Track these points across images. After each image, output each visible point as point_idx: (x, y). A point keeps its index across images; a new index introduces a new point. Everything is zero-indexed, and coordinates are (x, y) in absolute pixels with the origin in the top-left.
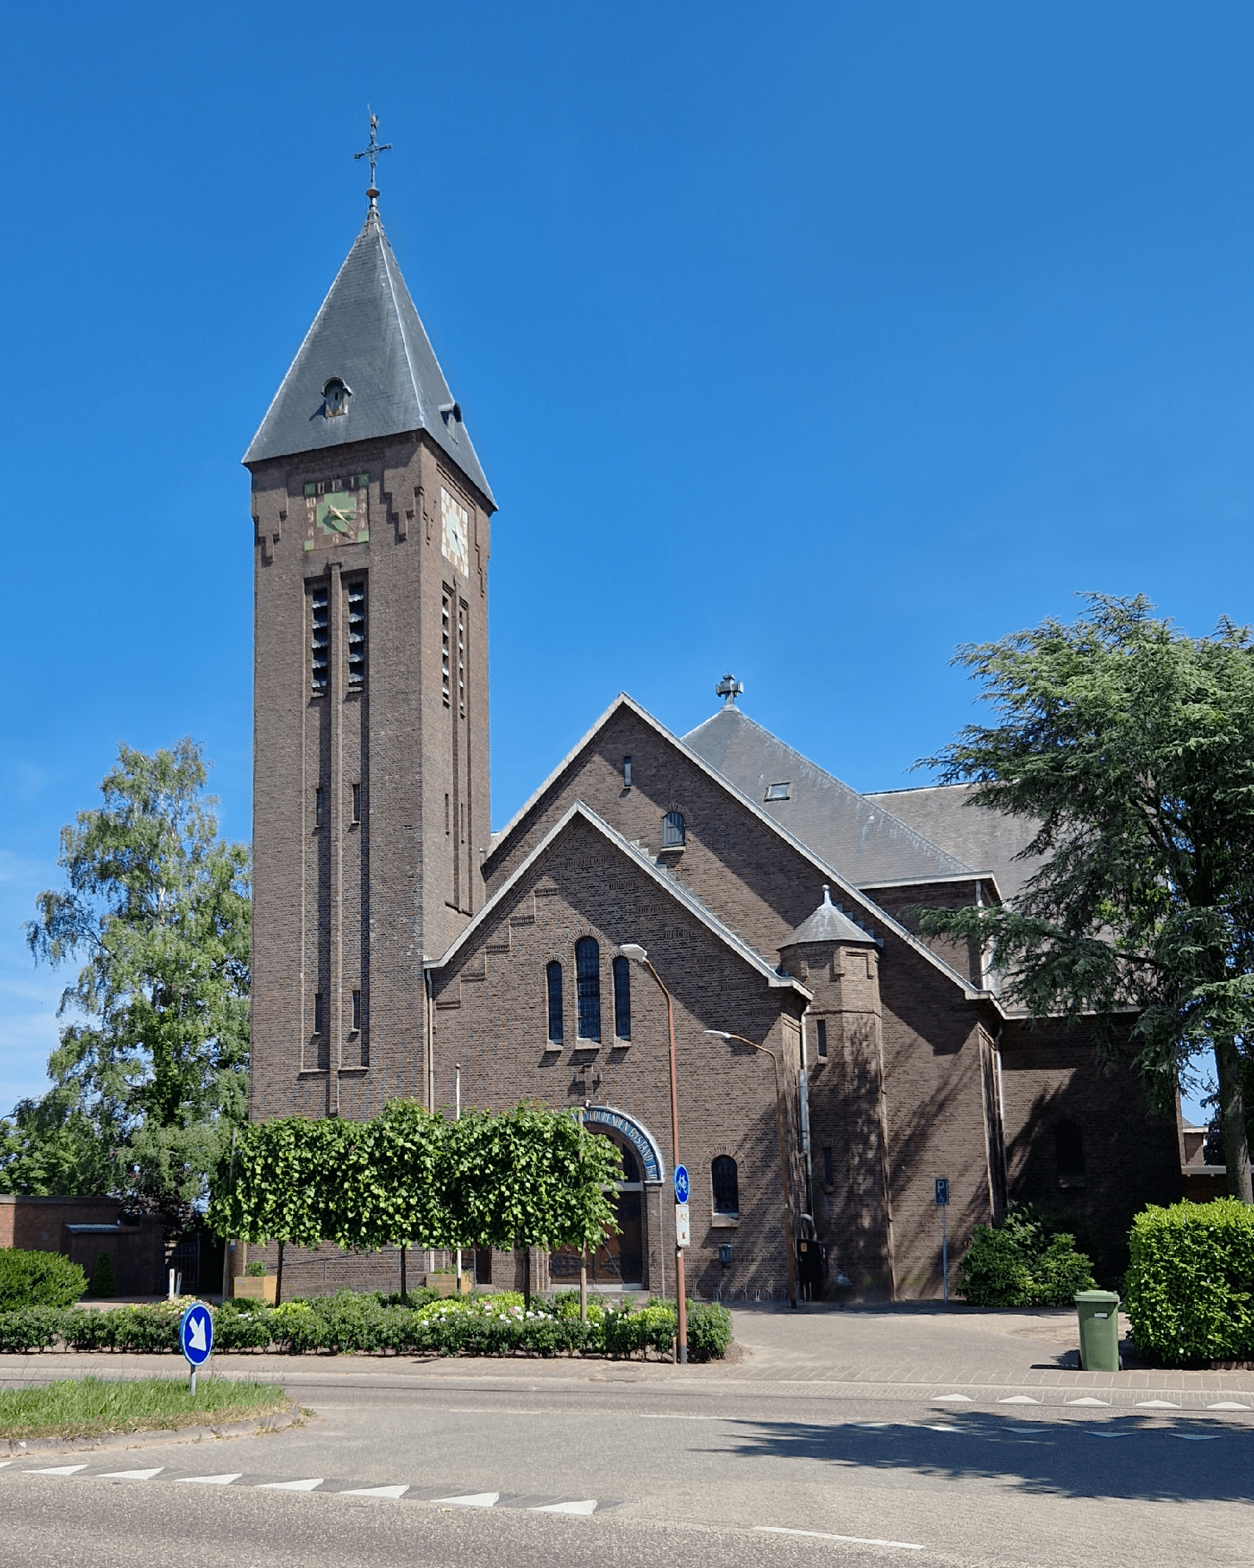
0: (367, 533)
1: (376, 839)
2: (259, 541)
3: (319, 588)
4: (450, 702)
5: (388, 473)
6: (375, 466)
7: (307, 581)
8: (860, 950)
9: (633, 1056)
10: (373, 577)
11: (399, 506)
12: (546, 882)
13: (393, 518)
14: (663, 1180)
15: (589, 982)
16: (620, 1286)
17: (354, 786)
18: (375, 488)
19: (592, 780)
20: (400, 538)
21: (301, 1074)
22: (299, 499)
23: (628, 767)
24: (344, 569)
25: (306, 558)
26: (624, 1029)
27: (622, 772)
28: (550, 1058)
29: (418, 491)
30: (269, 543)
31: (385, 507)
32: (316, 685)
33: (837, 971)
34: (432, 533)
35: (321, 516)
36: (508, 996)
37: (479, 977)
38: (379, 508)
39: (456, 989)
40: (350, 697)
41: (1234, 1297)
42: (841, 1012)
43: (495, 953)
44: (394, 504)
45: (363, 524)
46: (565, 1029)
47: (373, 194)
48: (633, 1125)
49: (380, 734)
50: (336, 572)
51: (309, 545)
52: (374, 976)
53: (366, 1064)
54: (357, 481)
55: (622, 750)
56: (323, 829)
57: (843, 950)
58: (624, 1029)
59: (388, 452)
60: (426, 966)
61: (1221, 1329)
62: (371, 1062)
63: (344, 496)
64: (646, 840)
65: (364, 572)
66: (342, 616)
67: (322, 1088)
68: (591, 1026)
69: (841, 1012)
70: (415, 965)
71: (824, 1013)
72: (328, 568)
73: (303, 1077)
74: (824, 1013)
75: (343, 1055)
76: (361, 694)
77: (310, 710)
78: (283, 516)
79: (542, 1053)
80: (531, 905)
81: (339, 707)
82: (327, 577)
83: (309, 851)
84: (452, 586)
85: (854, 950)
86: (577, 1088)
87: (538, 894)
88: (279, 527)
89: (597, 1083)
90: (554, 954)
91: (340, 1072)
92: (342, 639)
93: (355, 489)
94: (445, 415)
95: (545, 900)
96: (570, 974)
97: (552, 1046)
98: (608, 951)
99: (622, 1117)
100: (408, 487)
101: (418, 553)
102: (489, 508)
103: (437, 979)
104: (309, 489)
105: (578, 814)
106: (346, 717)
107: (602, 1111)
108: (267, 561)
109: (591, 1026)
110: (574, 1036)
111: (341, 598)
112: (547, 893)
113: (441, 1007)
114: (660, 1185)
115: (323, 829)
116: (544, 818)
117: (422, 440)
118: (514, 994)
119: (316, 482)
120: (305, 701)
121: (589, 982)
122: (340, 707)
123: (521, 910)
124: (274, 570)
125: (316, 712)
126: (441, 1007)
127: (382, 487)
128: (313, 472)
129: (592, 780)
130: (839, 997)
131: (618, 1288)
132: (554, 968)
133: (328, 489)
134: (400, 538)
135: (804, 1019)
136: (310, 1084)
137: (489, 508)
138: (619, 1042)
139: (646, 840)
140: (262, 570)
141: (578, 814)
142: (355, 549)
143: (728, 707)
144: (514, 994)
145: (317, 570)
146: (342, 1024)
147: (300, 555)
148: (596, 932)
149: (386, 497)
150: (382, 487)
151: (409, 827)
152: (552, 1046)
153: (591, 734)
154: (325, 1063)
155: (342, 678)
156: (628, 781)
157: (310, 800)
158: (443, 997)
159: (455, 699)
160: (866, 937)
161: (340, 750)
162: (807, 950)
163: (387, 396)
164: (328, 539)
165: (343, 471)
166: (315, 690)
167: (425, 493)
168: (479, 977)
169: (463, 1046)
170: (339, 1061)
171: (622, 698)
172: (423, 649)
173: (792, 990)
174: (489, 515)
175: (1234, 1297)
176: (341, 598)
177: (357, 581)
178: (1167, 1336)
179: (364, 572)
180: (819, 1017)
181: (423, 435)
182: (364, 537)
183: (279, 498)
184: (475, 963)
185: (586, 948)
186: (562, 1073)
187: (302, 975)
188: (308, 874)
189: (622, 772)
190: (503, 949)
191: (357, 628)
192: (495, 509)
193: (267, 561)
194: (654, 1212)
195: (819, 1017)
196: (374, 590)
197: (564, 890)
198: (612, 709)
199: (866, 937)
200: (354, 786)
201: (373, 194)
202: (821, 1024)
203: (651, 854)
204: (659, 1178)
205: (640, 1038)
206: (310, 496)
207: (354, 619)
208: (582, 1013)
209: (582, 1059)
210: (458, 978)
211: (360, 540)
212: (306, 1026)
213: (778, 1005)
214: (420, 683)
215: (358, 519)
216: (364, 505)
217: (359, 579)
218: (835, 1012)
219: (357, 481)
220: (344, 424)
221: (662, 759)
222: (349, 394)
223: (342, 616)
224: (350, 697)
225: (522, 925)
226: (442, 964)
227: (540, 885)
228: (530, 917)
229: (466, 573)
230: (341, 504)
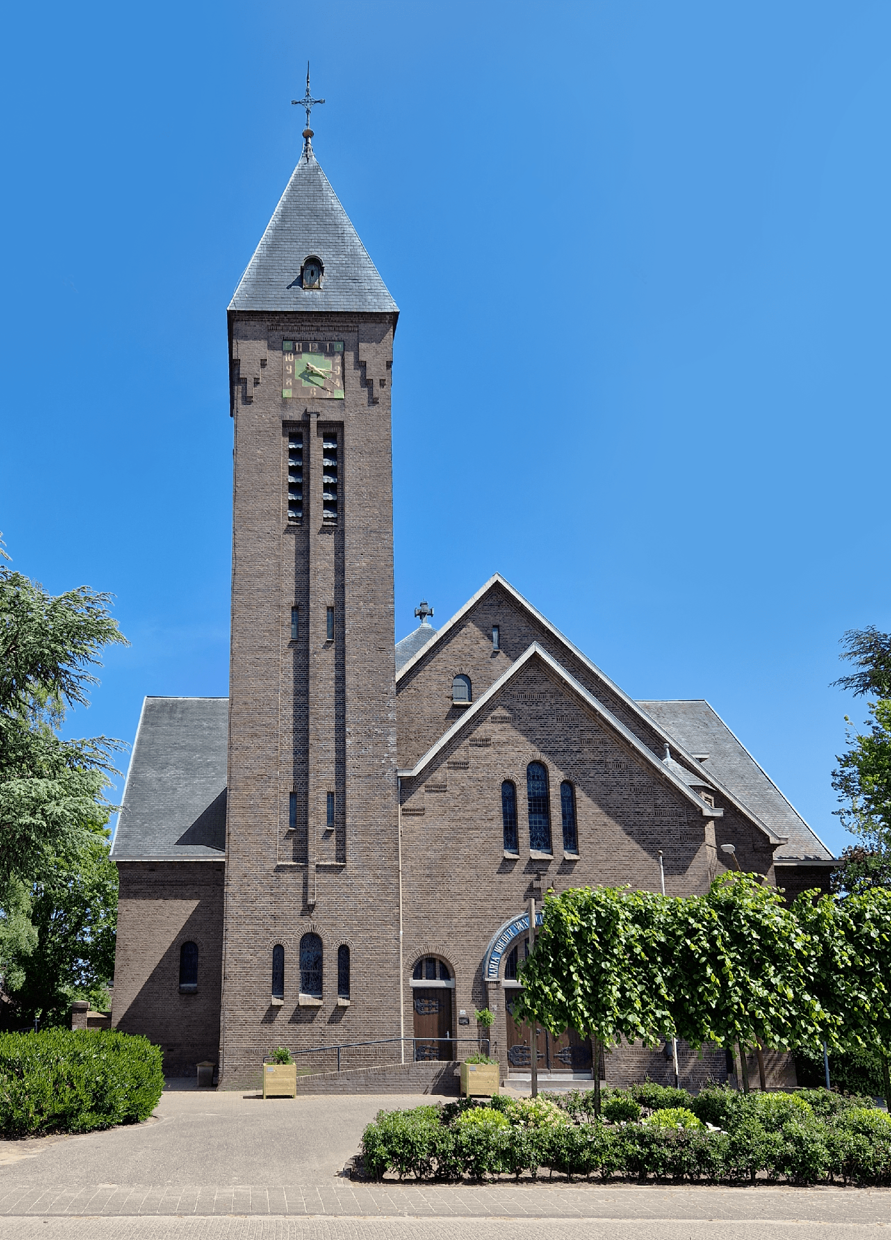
1: (351, 656)
3: (296, 431)
5: (362, 345)
6: (351, 337)
7: (286, 424)
10: (347, 431)
11: (373, 372)
12: (500, 712)
13: (367, 383)
15: (540, 804)
16: (572, 1075)
17: (328, 608)
18: (350, 357)
19: (467, 642)
20: (373, 401)
21: (278, 866)
22: (278, 353)
23: (495, 634)
24: (321, 418)
25: (285, 401)
27: (490, 637)
28: (507, 865)
29: (389, 365)
31: (359, 373)
32: (291, 514)
35: (299, 370)
36: (468, 808)
37: (441, 788)
38: (353, 375)
39: (418, 798)
43: (455, 768)
44: (368, 372)
45: (338, 383)
49: (356, 564)
50: (313, 420)
51: (287, 393)
52: (351, 782)
54: (331, 346)
55: (492, 620)
59: (363, 327)
62: (348, 858)
63: (322, 358)
65: (341, 425)
66: (318, 461)
67: (300, 881)
68: (542, 839)
72: (307, 415)
73: (279, 869)
75: (321, 851)
76: (336, 528)
78: (263, 363)
79: (501, 860)
82: (305, 423)
87: (494, 720)
88: (260, 373)
90: (509, 774)
91: (317, 866)
93: (331, 354)
95: (500, 726)
97: (509, 855)
98: (556, 776)
100: (381, 360)
104: (288, 345)
105: (535, 654)
111: (318, 446)
112: (503, 720)
113: (406, 813)
116: (427, 668)
118: (474, 805)
119: (294, 340)
121: (540, 804)
125: (291, 542)
127: (357, 356)
128: (292, 331)
129: (467, 642)
131: (569, 1077)
132: (509, 786)
133: (306, 350)
134: (373, 401)
136: (287, 878)
141: (535, 654)
142: (331, 403)
144: (474, 805)
146: (318, 823)
147: (279, 400)
148: (545, 759)
149: (361, 365)
150: (357, 356)
151: (381, 649)
153: (471, 603)
154: (302, 856)
155: (319, 515)
156: (496, 645)
164: (306, 390)
165: (320, 336)
166: (290, 519)
168: (441, 788)
169: (427, 850)
171: (496, 578)
176: (318, 446)
177: (333, 431)
179: (341, 425)
182: (339, 394)
184: (438, 776)
185: (537, 772)
186: (518, 880)
188: (287, 681)
189: (490, 637)
190: (464, 766)
197: (515, 719)
198: (489, 585)
200: (328, 608)
205: (587, 852)
206: (288, 352)
207: (328, 463)
209: (536, 868)
210: (422, 789)
212: (281, 820)
216: (339, 368)
217: (332, 430)
219: (331, 346)
220: (322, 297)
223: (318, 461)
224: (324, 530)
225: (480, 746)
226: (415, 773)
227: (495, 713)
228: (487, 740)
230: (322, 365)
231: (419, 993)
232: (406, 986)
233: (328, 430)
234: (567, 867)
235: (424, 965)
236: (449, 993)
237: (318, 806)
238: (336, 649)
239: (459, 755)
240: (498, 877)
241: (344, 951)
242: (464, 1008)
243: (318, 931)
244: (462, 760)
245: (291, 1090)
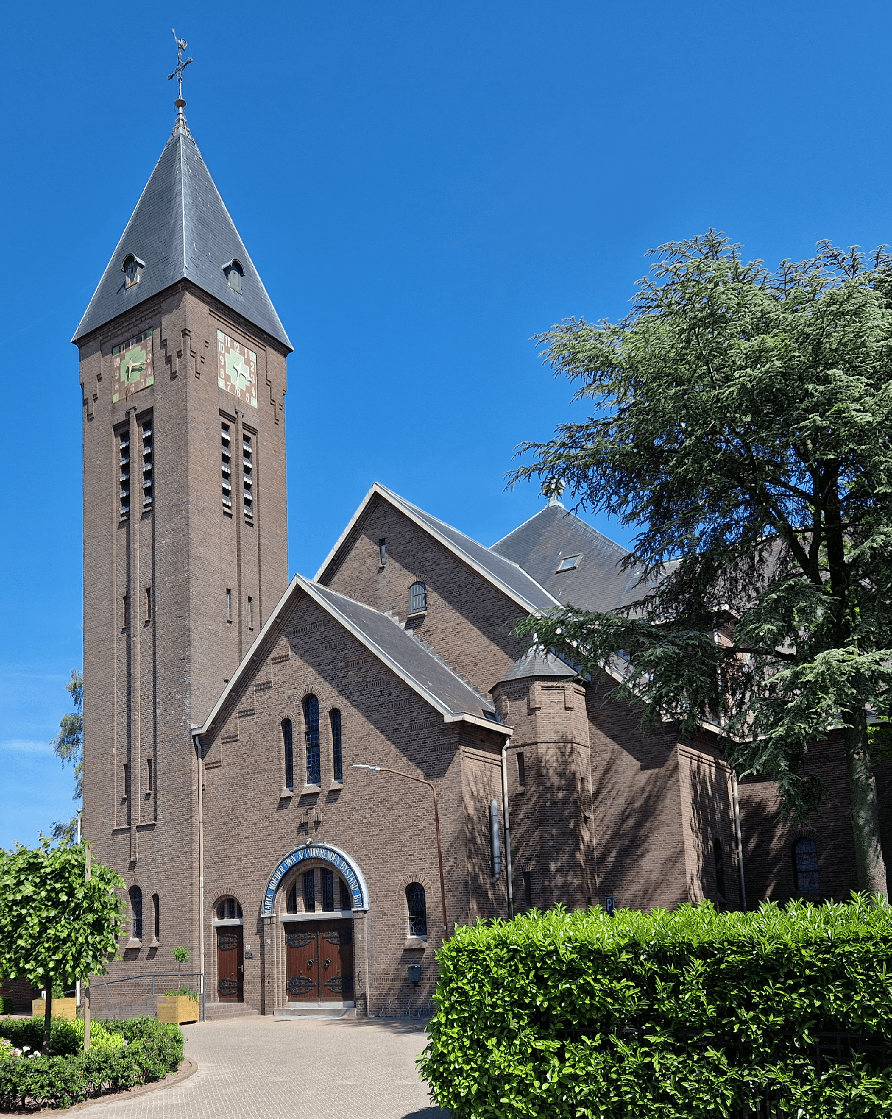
0: (152, 377)
2: (85, 402)
3: (122, 431)
4: (233, 512)
8: (554, 684)
9: (345, 796)
14: (366, 907)
20: (174, 376)
24: (138, 411)
26: (338, 775)
30: (90, 402)
33: (533, 705)
34: (203, 369)
37: (234, 739)
39: (217, 750)
40: (144, 515)
41: (540, 1045)
42: (536, 743)
45: (150, 371)
46: (294, 777)
47: (181, 103)
48: (343, 859)
49: (163, 542)
50: (133, 415)
51: (116, 398)
53: (155, 819)
56: (127, 629)
57: (538, 685)
58: (338, 775)
60: (194, 733)
61: (523, 1089)
64: (396, 609)
68: (315, 775)
69: (536, 743)
70: (186, 733)
71: (523, 746)
72: (128, 413)
73: (116, 832)
74: (523, 746)
75: (141, 813)
76: (149, 512)
77: (120, 532)
80: (268, 672)
81: (136, 525)
83: (119, 648)
84: (234, 414)
85: (550, 684)
86: (303, 827)
87: (275, 661)
89: (317, 823)
91: (137, 827)
92: (138, 468)
94: (227, 271)
96: (300, 728)
99: (334, 852)
101: (186, 386)
102: (285, 351)
103: (203, 742)
106: (141, 533)
107: (320, 847)
108: (90, 417)
109: (315, 775)
110: (302, 781)
113: (208, 767)
114: (365, 912)
115: (127, 629)
117: (187, 290)
120: (115, 525)
122: (137, 526)
123: (261, 677)
124: (95, 423)
126: (208, 767)
130: (534, 728)
132: (287, 724)
135: (504, 753)
137: (285, 351)
138: (335, 785)
139: (396, 609)
140: (88, 425)
143: (552, 504)
145: (121, 417)
152: (286, 793)
153: (352, 523)
155: (138, 501)
157: (119, 607)
158: (210, 757)
159: (238, 508)
160: (567, 671)
161: (137, 562)
162: (507, 689)
163: (166, 259)
167: (192, 334)
168: (234, 739)
170: (139, 818)
172: (191, 466)
173: (463, 722)
174: (285, 356)
175: (540, 1045)
176: (137, 433)
177: (146, 419)
178: (457, 1096)
180: (519, 750)
181: (186, 284)
183: (97, 361)
184: (229, 727)
186: (292, 815)
187: (114, 751)
188: (118, 667)
191: (149, 458)
192: (291, 351)
193: (90, 417)
194: (359, 936)
195: (519, 750)
196: (157, 423)
198: (367, 499)
199: (567, 671)
201: (181, 103)
202: (520, 756)
203: (400, 621)
204: (363, 906)
207: (147, 451)
208: (309, 763)
209: (308, 800)
211: (148, 385)
213: (456, 739)
214: (188, 495)
215: (146, 369)
217: (148, 418)
218: (532, 744)
221: (408, 536)
222: (142, 266)
229: (254, 403)
230: (136, 356)
231: (220, 930)
232: (207, 927)
233: (144, 420)
234: (332, 797)
235: (226, 905)
236: (240, 928)
237: (140, 771)
238: (435, 590)
239: (244, 703)
240: (276, 816)
241: (156, 898)
242: (250, 943)
243: (138, 884)
244: (248, 708)
245: (197, 1019)
